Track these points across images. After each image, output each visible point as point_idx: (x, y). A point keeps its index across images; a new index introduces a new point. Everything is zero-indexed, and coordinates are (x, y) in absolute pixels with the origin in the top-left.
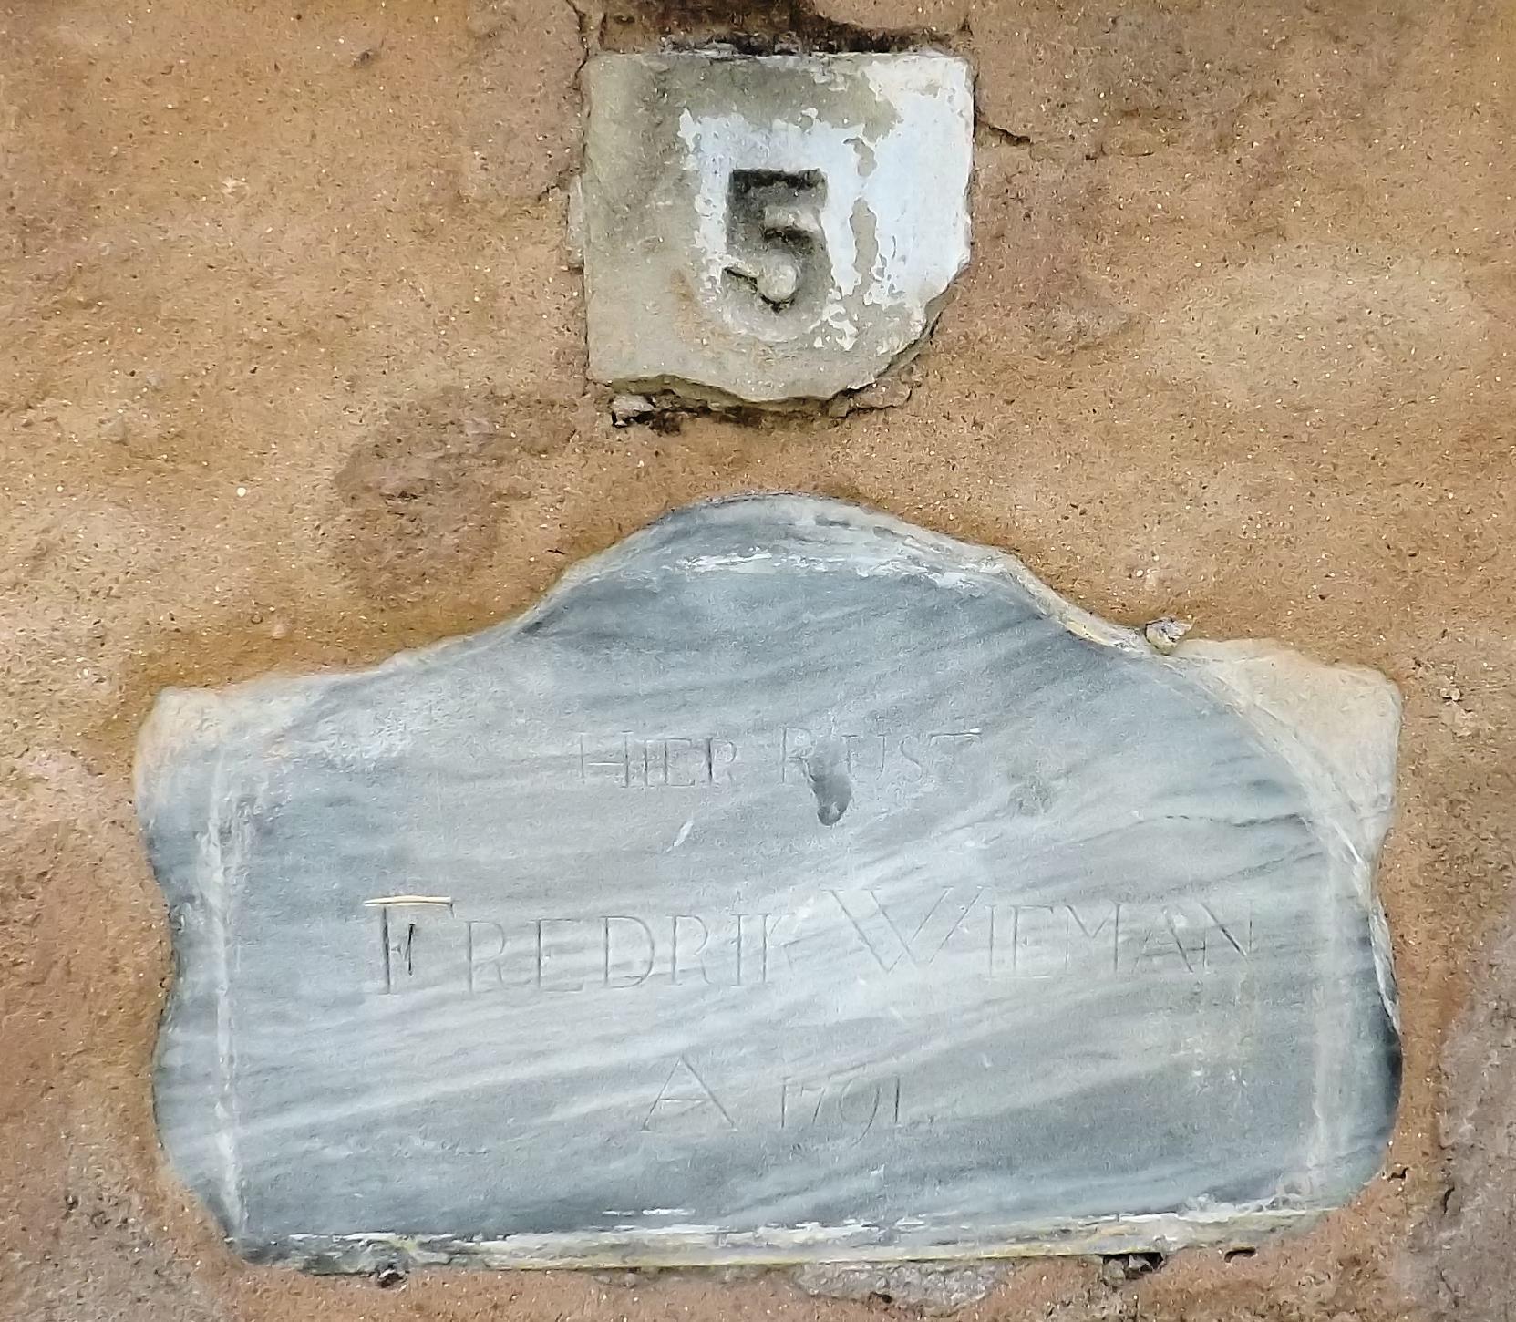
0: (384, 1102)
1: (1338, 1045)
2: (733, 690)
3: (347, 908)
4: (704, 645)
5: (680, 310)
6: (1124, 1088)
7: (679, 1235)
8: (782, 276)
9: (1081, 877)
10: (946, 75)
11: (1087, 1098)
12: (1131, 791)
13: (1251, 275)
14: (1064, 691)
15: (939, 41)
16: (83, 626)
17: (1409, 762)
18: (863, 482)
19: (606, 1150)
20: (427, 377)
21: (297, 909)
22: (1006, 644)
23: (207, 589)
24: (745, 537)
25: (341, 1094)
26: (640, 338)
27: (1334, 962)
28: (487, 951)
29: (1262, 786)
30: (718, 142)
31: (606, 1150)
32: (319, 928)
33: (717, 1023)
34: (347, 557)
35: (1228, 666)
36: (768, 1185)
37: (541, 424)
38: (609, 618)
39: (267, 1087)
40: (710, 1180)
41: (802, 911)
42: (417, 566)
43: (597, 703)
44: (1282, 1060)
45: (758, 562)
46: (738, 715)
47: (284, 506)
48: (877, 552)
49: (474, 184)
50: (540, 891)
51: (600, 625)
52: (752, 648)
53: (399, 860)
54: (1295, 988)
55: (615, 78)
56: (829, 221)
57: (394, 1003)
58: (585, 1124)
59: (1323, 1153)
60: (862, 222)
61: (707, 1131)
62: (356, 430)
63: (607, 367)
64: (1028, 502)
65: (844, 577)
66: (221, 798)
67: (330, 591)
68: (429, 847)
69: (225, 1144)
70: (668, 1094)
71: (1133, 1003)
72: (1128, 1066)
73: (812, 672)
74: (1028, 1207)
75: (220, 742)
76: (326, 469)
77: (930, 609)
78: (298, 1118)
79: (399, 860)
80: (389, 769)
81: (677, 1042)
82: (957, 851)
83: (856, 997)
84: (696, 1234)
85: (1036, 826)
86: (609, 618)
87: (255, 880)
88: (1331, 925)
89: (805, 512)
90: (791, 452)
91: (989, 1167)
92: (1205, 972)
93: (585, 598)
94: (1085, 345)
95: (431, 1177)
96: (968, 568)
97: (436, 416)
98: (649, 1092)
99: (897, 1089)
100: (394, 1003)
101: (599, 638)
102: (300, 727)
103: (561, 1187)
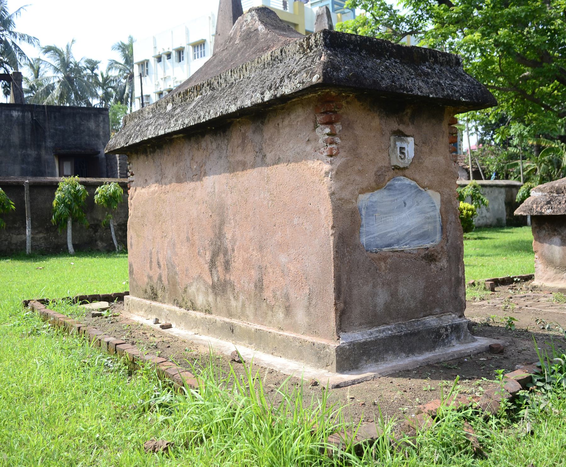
0: (375, 235)
1: (439, 228)
2: (398, 194)
3: (373, 215)
4: (396, 190)
5: (396, 161)
6: (425, 231)
7: (396, 247)
8: (403, 157)
9: (422, 212)
10: (413, 139)
11: (423, 232)
12: (424, 204)
13: (431, 157)
14: (419, 194)
15: (412, 137)
16: (357, 187)
17: (442, 201)
18: (407, 175)
19: (391, 239)
20: (380, 165)
21: (369, 216)
22: (416, 190)
23: (365, 184)
24: (399, 180)
25: (372, 234)
26: (394, 162)
27: (438, 219)
28: (383, 219)
29: (433, 203)
30: (399, 144)
31: (391, 239)
32: (371, 217)
33: (399, 226)
34: (375, 181)
35: (430, 192)
36: (402, 242)
37: (388, 169)
38: (390, 187)
39: (368, 233)
40: (398, 242)
41: (404, 215)
42: (378, 184)
43: (390, 195)
44: (435, 228)
45: (399, 182)
46: (399, 196)
47: (369, 178)
48: (407, 181)
49: (383, 147)
50: (386, 214)
51: (389, 188)
52: (399, 190)
53: (376, 210)
54: (435, 222)
55: (392, 138)
56: (406, 152)
57: (376, 225)
58: (390, 236)
59: (438, 238)
60: (408, 152)
61: (398, 237)
62: (375, 169)
63: (392, 164)
64: (417, 177)
65: (405, 184)
66: (364, 205)
67: (373, 184)
68: (378, 209)
69: (364, 239)
70: (395, 233)
71: (425, 223)
72: (425, 230)
73: (403, 193)
74: (419, 243)
75: (364, 199)
76: (373, 173)
77: (411, 187)
78: (369, 237)
79: (376, 210)
80: (376, 202)
81: (396, 228)
82: (413, 209)
83: (408, 223)
84: (397, 247)
85: (418, 207)
86: (390, 187)
87: (366, 212)
88: (438, 216)
89: (402, 178)
90: (400, 173)
91: (417, 239)
92: (430, 220)
93: (389, 186)
94: (421, 163)
95: (379, 242)
96: (413, 183)
97: (381, 168)
98: (392, 234)
99: (410, 232)
100: (376, 225)
101: (389, 189)
102: (369, 198)
103: (388, 243)
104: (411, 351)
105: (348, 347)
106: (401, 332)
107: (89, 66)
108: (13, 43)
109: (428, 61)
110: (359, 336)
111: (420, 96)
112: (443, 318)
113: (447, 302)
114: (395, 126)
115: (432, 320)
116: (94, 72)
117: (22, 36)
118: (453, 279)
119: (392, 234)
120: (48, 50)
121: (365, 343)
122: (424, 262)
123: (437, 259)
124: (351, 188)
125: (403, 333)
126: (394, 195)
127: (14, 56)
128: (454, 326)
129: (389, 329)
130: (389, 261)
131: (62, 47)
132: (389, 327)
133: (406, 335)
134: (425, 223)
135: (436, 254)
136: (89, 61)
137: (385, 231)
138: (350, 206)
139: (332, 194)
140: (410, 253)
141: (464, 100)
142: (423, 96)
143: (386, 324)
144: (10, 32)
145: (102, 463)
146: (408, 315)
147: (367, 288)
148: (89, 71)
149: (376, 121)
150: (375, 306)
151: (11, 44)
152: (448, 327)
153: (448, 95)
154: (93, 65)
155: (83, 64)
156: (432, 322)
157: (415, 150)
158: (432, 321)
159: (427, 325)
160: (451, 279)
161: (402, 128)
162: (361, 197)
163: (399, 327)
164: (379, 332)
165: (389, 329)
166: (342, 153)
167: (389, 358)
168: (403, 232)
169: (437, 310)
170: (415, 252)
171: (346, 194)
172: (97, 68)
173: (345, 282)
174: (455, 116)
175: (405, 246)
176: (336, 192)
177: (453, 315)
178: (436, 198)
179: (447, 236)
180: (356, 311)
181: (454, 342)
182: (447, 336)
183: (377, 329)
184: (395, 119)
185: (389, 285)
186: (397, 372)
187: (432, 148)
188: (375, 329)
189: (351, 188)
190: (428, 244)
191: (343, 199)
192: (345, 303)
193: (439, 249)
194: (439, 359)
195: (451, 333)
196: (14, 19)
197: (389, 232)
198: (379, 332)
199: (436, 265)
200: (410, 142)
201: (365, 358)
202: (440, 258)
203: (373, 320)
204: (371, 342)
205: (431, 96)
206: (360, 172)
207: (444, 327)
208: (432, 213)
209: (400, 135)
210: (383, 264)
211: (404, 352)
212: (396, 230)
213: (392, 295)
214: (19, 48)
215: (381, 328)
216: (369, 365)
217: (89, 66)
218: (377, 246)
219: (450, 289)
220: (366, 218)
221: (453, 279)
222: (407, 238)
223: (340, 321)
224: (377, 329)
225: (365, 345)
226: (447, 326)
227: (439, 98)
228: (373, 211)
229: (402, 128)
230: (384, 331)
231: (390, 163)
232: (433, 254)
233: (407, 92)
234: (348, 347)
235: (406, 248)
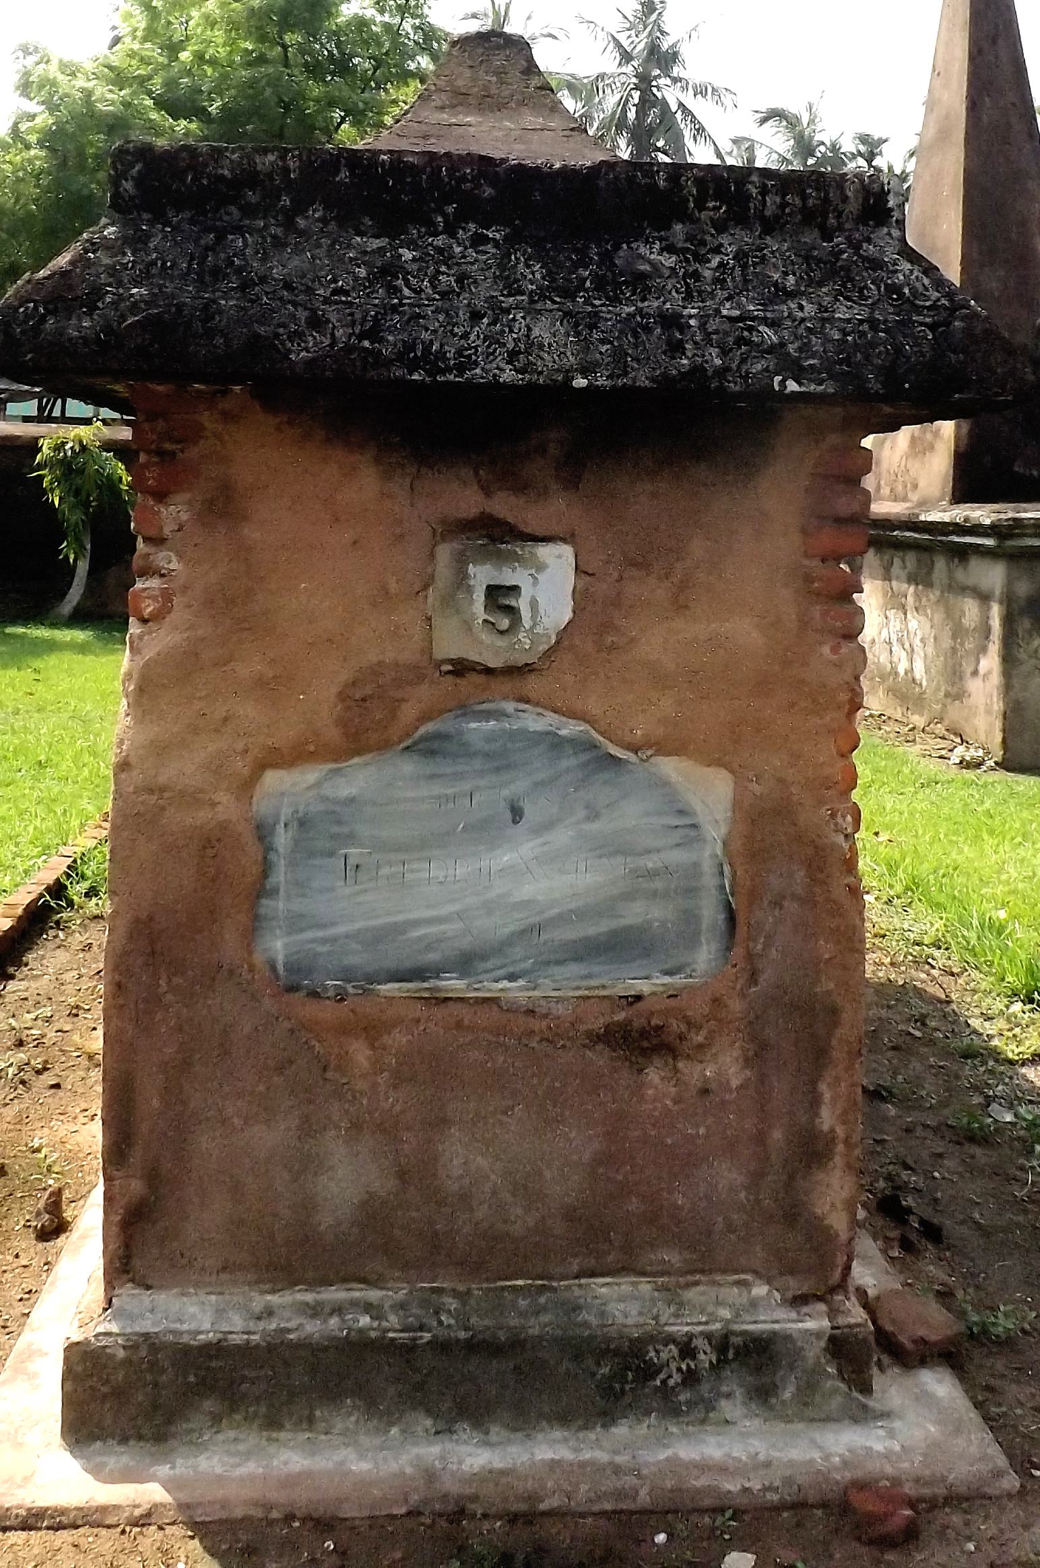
1: (710, 913)
3: (331, 854)
7: (453, 984)
8: (505, 623)
10: (567, 551)
12: (632, 814)
15: (564, 540)
16: (240, 746)
17: (736, 805)
18: (533, 695)
21: (312, 854)
22: (584, 757)
25: (323, 926)
29: (681, 812)
30: (482, 575)
35: (669, 767)
36: (489, 965)
40: (465, 963)
41: (506, 858)
43: (433, 776)
44: (690, 918)
48: (536, 722)
51: (430, 748)
52: (487, 756)
55: (445, 553)
56: (523, 604)
57: (347, 891)
58: (420, 939)
60: (534, 604)
61: (466, 943)
62: (345, 676)
64: (593, 705)
67: (333, 734)
68: (363, 830)
70: (450, 928)
71: (629, 896)
73: (508, 767)
74: (589, 976)
75: (287, 789)
77: (555, 743)
80: (352, 800)
81: (456, 907)
82: (562, 836)
83: (527, 890)
85: (595, 826)
87: (296, 842)
89: (510, 706)
90: (506, 685)
94: (613, 648)
95: (357, 958)
99: (539, 928)
101: (432, 753)
102: (318, 784)
104: (467, 1410)
105: (121, 1354)
106: (421, 1328)
107: (862, 148)
108: (681, 105)
109: (685, 217)
110: (195, 1314)
111: (511, 387)
112: (691, 1294)
113: (730, 1228)
114: (467, 500)
115: (622, 1299)
116: (874, 163)
117: (700, 91)
118: (777, 1135)
119: (433, 929)
120: (774, 114)
121: (216, 1350)
122: (600, 1058)
123: (685, 1047)
124: (208, 747)
125: (427, 1336)
126: (458, 776)
127: (679, 137)
128: (735, 1340)
129: (368, 1308)
130: (398, 1039)
131: (795, 107)
132: (374, 1295)
133: (442, 1347)
134: (629, 896)
135: (676, 1026)
136: (864, 139)
137: (400, 918)
138: (202, 816)
139: (123, 766)
140: (531, 1012)
141: (792, 386)
142: (531, 386)
143: (363, 1280)
144: (676, 80)
145: (1033, 1042)
146: (491, 1256)
147: (271, 1137)
148: (861, 162)
149: (362, 485)
150: (308, 1206)
151: (674, 107)
152: (699, 1343)
153: (697, 370)
154: (871, 147)
155: (849, 146)
156: (616, 1310)
157: (581, 599)
158: (620, 1303)
159: (584, 1316)
160: (760, 1138)
161: (503, 506)
162: (273, 779)
163: (424, 1303)
164: (315, 1311)
165: (368, 1308)
166: (179, 615)
167: (339, 1425)
168: (503, 926)
169: (672, 1257)
170: (560, 1010)
171: (184, 769)
172: (881, 153)
173: (155, 1103)
174: (868, 442)
175: (505, 984)
176: (133, 760)
177: (760, 1290)
178: (711, 795)
179: (750, 956)
180: (205, 1218)
181: (730, 1408)
182: (691, 1379)
183: (309, 1297)
184: (466, 472)
185: (388, 1129)
186: (275, 1514)
187: (684, 585)
188: (300, 1297)
189: (208, 747)
190: (648, 982)
191: (162, 789)
192: (153, 1177)
193: (698, 1008)
194: (533, 1498)
195: (715, 1368)
196: (685, 51)
197: (416, 923)
198: (315, 1311)
199: (676, 1070)
200: (550, 561)
201: (209, 1405)
202: (700, 1046)
203: (291, 1257)
204: (246, 1350)
205: (580, 382)
206: (270, 688)
207: (670, 1339)
208: (677, 857)
209: (497, 536)
210: (360, 1053)
211: (429, 1412)
212: (459, 915)
213: (402, 1175)
214: (693, 116)
215: (335, 1294)
216: (232, 1434)
217: (862, 148)
218: (348, 975)
219: (756, 1178)
220: (292, 864)
221: (777, 1135)
222: (518, 951)
223: (127, 1246)
224: (309, 1297)
225: (210, 1357)
226: (690, 1336)
227: (632, 391)
228: (333, 837)
229: (503, 506)
230: (338, 1310)
231: (428, 650)
232: (659, 1028)
233: (434, 371)
234: (121, 1354)
235: (515, 991)
